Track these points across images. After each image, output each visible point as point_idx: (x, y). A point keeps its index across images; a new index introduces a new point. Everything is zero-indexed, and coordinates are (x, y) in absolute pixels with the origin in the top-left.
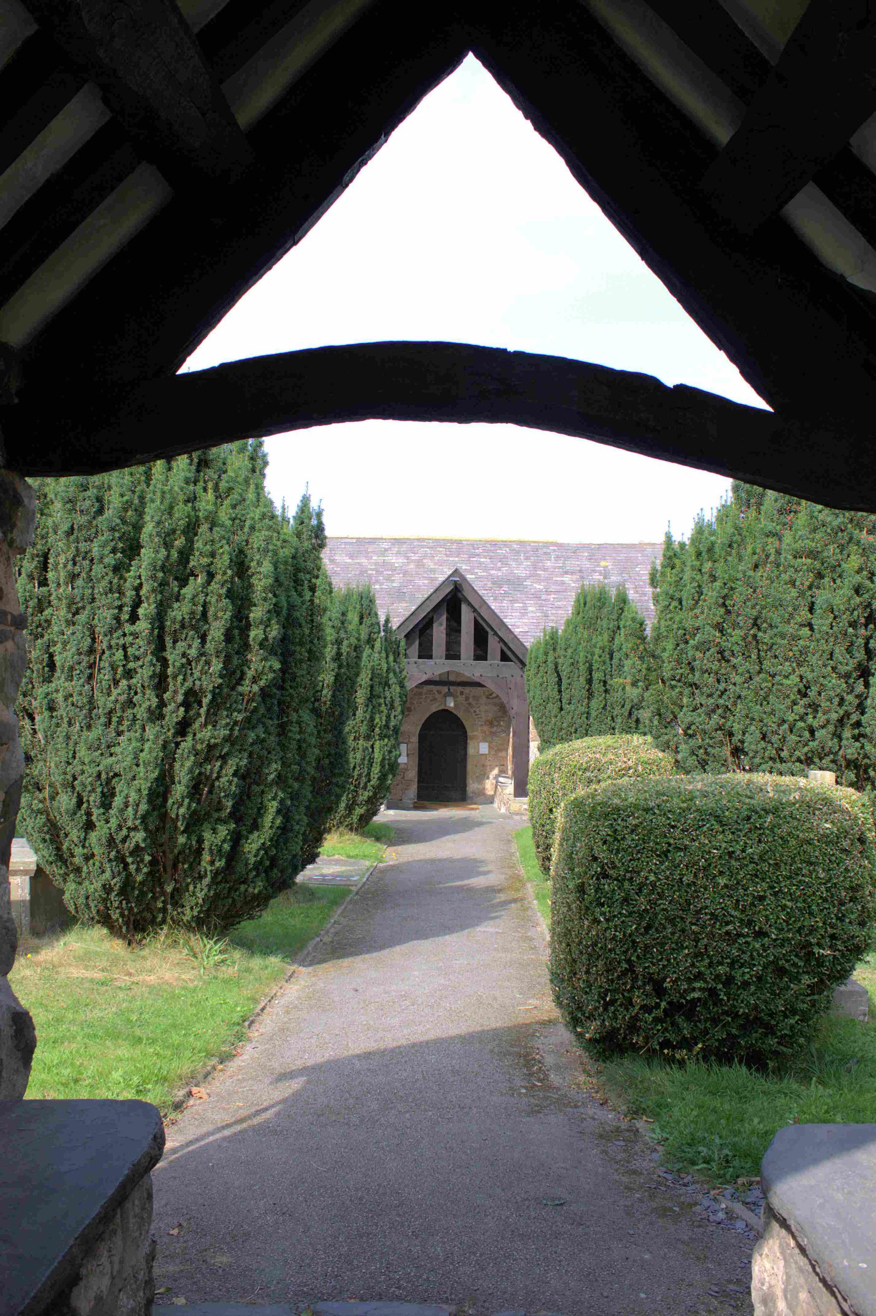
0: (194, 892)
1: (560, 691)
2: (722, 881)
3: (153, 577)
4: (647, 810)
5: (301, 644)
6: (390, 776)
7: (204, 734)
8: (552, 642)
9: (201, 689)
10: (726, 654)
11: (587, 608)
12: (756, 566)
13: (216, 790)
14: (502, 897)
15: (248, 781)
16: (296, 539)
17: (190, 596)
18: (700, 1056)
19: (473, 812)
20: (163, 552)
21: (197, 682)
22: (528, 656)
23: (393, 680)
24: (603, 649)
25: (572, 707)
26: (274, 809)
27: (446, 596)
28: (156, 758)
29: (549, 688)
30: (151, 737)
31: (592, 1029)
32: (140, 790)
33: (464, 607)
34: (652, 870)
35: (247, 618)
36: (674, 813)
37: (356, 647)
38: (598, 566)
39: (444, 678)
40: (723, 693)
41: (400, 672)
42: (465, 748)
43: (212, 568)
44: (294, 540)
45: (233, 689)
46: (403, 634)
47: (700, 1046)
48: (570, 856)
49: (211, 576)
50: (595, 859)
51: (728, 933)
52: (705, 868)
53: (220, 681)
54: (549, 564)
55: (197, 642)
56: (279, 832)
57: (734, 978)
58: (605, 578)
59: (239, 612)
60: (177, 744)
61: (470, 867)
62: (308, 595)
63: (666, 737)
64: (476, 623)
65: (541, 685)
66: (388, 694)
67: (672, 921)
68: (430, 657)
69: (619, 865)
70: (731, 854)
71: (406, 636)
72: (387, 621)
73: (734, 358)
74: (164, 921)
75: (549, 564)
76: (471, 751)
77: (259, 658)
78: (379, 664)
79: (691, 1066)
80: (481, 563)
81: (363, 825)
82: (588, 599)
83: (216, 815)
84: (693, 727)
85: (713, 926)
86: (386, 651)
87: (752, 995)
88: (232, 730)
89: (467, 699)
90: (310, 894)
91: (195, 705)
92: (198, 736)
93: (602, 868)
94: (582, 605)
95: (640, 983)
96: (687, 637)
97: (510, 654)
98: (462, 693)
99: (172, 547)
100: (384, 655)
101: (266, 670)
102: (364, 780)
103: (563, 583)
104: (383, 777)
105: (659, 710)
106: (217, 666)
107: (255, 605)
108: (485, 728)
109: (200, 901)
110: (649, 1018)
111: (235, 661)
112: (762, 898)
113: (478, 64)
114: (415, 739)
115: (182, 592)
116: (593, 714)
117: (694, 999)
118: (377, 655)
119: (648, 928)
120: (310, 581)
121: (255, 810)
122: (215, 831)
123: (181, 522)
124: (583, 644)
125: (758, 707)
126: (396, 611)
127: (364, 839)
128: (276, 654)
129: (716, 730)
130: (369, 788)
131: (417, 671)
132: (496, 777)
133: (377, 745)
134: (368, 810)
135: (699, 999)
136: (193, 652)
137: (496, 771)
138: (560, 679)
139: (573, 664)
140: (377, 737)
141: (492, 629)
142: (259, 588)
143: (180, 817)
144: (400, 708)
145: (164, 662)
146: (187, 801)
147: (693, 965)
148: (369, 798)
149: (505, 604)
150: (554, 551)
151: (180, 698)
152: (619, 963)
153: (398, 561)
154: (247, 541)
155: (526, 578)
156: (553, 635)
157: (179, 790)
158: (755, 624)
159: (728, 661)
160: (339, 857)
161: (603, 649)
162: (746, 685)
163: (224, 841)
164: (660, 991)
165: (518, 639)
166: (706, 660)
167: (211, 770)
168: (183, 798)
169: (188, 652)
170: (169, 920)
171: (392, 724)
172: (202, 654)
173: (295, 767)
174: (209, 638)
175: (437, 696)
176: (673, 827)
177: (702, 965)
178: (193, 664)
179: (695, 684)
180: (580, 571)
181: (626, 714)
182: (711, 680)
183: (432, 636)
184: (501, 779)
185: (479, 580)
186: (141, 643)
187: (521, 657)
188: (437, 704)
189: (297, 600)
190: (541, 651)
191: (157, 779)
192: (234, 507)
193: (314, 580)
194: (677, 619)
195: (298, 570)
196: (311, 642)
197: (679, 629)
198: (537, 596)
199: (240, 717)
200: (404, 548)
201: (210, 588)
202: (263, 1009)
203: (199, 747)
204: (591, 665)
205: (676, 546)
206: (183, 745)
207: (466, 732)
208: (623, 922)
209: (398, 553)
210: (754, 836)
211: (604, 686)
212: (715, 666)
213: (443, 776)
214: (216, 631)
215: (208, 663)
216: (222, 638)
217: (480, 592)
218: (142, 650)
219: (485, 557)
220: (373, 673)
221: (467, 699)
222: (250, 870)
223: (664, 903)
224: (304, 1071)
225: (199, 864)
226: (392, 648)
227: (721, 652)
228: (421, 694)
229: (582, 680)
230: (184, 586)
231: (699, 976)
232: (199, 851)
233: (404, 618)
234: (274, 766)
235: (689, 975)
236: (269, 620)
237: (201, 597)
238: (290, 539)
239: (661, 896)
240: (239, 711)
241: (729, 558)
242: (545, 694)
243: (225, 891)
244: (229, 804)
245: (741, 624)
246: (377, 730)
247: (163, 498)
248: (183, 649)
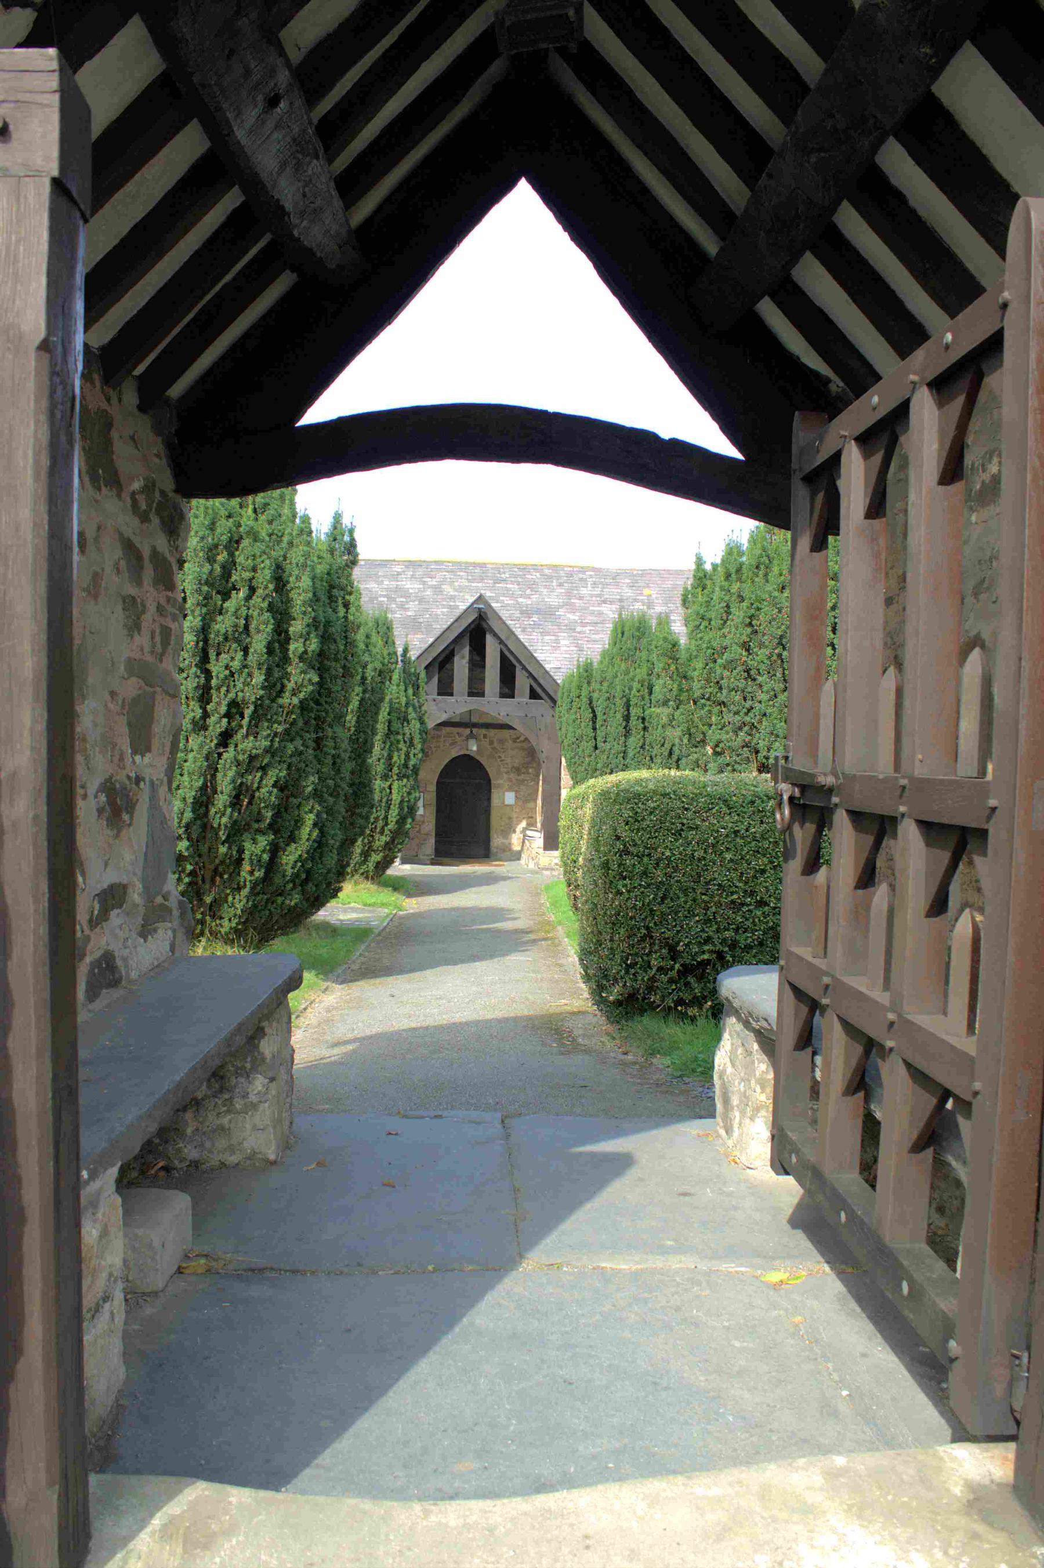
0: (232, 903)
1: (594, 729)
2: (728, 856)
3: (199, 591)
4: (665, 795)
5: (336, 660)
6: (409, 820)
7: (246, 745)
8: (585, 674)
9: (243, 700)
10: (752, 672)
13: (256, 800)
14: (532, 936)
15: (286, 792)
16: (329, 556)
17: (233, 610)
18: (709, 1013)
19: (499, 868)
20: (207, 568)
21: (240, 694)
22: (560, 694)
23: (412, 715)
24: (642, 682)
25: (608, 746)
26: (311, 822)
28: (200, 767)
30: (195, 748)
31: (614, 993)
32: (184, 799)
33: (489, 638)
34: (668, 848)
35: (287, 632)
36: (687, 797)
37: (380, 671)
38: (641, 594)
39: (467, 720)
40: (749, 711)
41: (420, 707)
42: (489, 799)
43: (254, 583)
44: (327, 556)
45: (273, 701)
46: (423, 666)
47: (709, 1003)
48: (597, 840)
49: (252, 590)
50: (618, 838)
51: (733, 902)
52: (713, 845)
53: (262, 692)
55: (240, 655)
56: (316, 845)
57: (738, 942)
58: (649, 608)
59: (279, 626)
60: (220, 755)
61: (498, 914)
62: (342, 611)
63: (696, 756)
64: (504, 659)
66: (407, 730)
67: (685, 891)
68: (452, 694)
69: (639, 842)
70: (736, 832)
71: (426, 668)
72: (406, 651)
73: (715, 416)
74: (202, 934)
75: (584, 591)
76: (495, 800)
77: (298, 671)
78: (398, 698)
79: (701, 1021)
80: (508, 589)
81: (378, 874)
82: (626, 629)
83: (256, 826)
84: (721, 745)
85: (720, 896)
86: (405, 683)
87: (754, 956)
88: (272, 741)
89: (491, 743)
90: (332, 931)
91: (237, 716)
92: (240, 747)
93: (625, 846)
94: (620, 635)
95: (657, 947)
96: (716, 656)
98: (485, 736)
99: (215, 561)
100: (402, 687)
101: (306, 682)
102: (380, 823)
103: (600, 613)
104: (401, 821)
105: (689, 729)
106: (259, 678)
107: (294, 619)
108: (512, 775)
109: (239, 912)
110: (664, 978)
111: (277, 674)
112: (763, 872)
114: (433, 788)
115: (225, 605)
117: (703, 960)
118: (395, 687)
119: (663, 898)
120: (344, 598)
121: (292, 823)
122: (254, 841)
123: (224, 537)
124: (620, 677)
125: (783, 724)
126: (416, 641)
127: (381, 889)
128: (313, 668)
129: (743, 747)
130: (387, 832)
131: (438, 709)
132: (525, 830)
134: (385, 857)
135: (709, 961)
136: (236, 664)
137: (524, 824)
138: (595, 716)
140: (395, 777)
142: (299, 602)
143: (223, 827)
144: (419, 746)
145: (208, 673)
146: (229, 810)
147: (703, 930)
148: (387, 843)
149: (535, 636)
151: (223, 709)
152: (639, 929)
153: (412, 587)
154: (285, 558)
155: (560, 607)
157: (222, 800)
158: (780, 643)
159: (754, 680)
160: (354, 904)
161: (642, 682)
162: (771, 703)
163: (264, 851)
164: (674, 954)
165: (550, 676)
166: (733, 679)
167: (253, 780)
168: (225, 807)
169: (231, 664)
170: (207, 932)
171: (412, 763)
172: (245, 666)
173: (331, 782)
174: (252, 650)
176: (686, 809)
177: (711, 931)
178: (236, 676)
179: (723, 703)
180: (621, 600)
181: (666, 754)
182: (738, 698)
183: (453, 670)
184: (529, 833)
185: (506, 608)
186: (186, 656)
187: (552, 694)
188: (457, 748)
189: (333, 617)
190: (574, 684)
191: (201, 789)
192: (270, 522)
193: (347, 597)
194: (706, 638)
195: (332, 587)
196: (346, 658)
197: (708, 648)
198: (570, 628)
199: (280, 729)
200: (420, 572)
201: (252, 602)
202: (305, 1009)
203: (241, 758)
204: (628, 701)
205: (708, 567)
206: (225, 755)
208: (642, 893)
209: (413, 576)
210: (757, 818)
211: (643, 723)
212: (742, 684)
213: (464, 828)
214: (259, 643)
215: (250, 675)
216: (265, 650)
217: (509, 622)
218: (187, 662)
219: (512, 583)
220: (391, 707)
221: (491, 743)
222: (288, 882)
223: (678, 876)
224: (354, 1040)
225: (239, 874)
226: (411, 681)
227: (748, 671)
228: (439, 737)
229: (619, 716)
230: (227, 600)
231: (708, 940)
232: (239, 861)
233: (420, 652)
234: (312, 778)
235: (699, 939)
236: (308, 633)
237: (244, 611)
238: (325, 555)
239: (676, 869)
240: (280, 724)
241: (756, 579)
243: (263, 903)
244: (269, 814)
245: (767, 643)
246: (395, 770)
247: (206, 513)
248: (225, 662)
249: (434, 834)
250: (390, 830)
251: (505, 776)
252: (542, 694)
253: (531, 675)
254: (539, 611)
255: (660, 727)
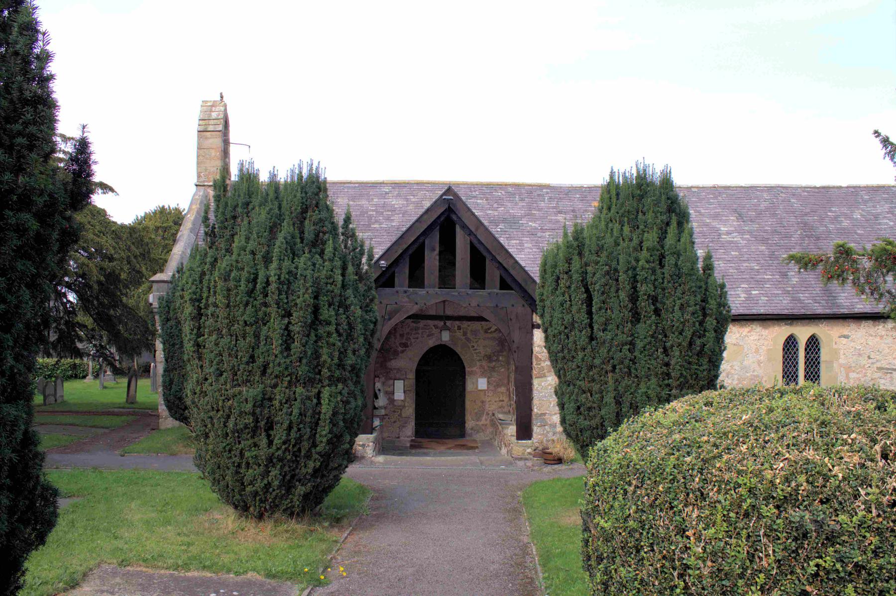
1: (590, 313)
8: (575, 244)
11: (621, 201)
27: (439, 217)
29: (574, 309)
54: (542, 204)
65: (562, 305)
75: (542, 204)
76: (469, 387)
89: (465, 334)
94: (614, 200)
97: (512, 280)
102: (305, 445)
108: (484, 363)
114: (412, 376)
116: (640, 344)
133: (326, 393)
134: (315, 487)
139: (608, 273)
140: (326, 382)
141: (491, 253)
148: (316, 471)
150: (547, 193)
153: (397, 203)
155: (522, 217)
156: (578, 234)
175: (434, 331)
180: (573, 211)
181: (685, 344)
188: (434, 339)
198: (532, 233)
207: (464, 368)
221: (465, 334)
228: (417, 329)
242: (568, 318)
249: (413, 417)
250: (319, 453)
251: (478, 363)
252: (513, 285)
253: (501, 265)
254: (504, 221)
255: (677, 308)
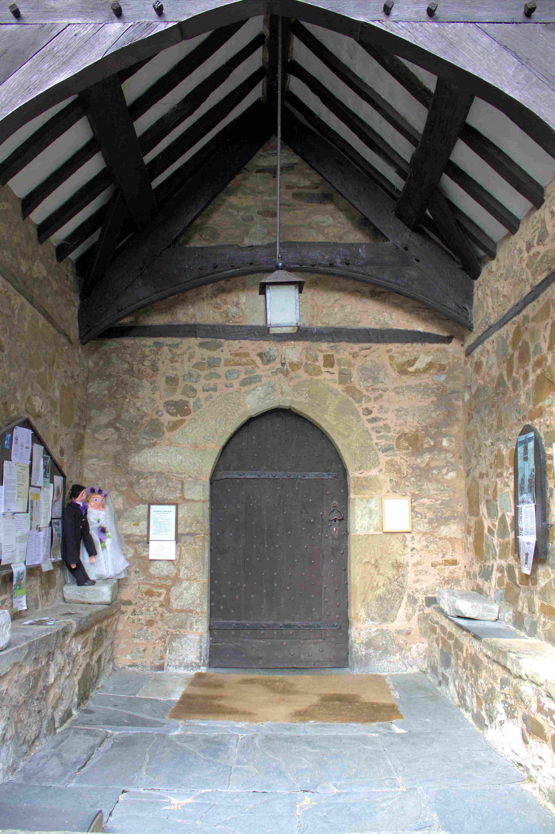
12: (408, 633)
42: (343, 519)
89: (344, 377)
108: (400, 458)
113: (417, 128)
114: (199, 492)
207: (344, 472)
